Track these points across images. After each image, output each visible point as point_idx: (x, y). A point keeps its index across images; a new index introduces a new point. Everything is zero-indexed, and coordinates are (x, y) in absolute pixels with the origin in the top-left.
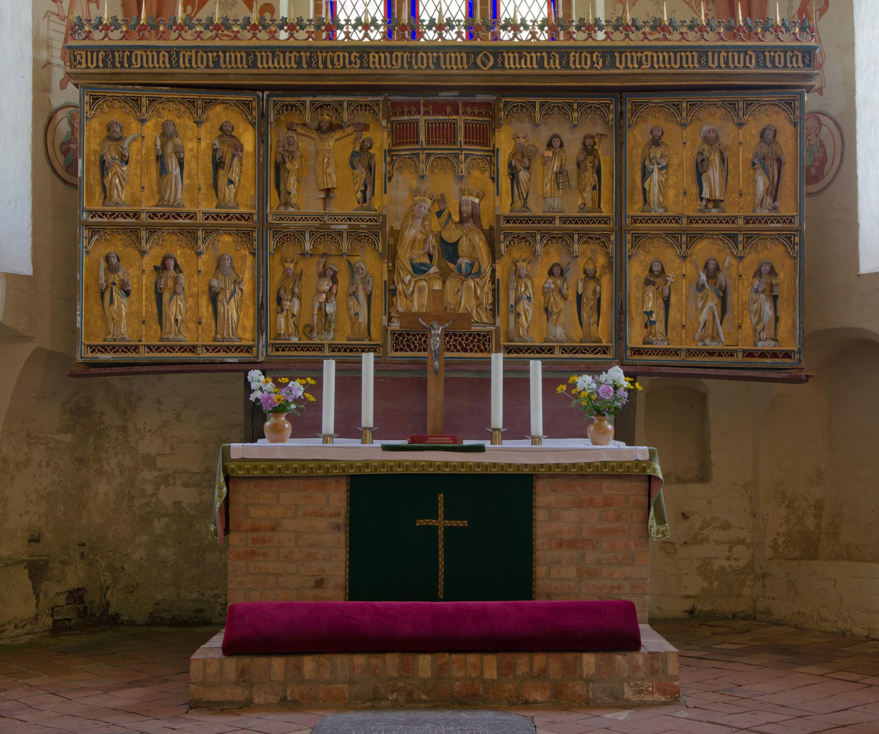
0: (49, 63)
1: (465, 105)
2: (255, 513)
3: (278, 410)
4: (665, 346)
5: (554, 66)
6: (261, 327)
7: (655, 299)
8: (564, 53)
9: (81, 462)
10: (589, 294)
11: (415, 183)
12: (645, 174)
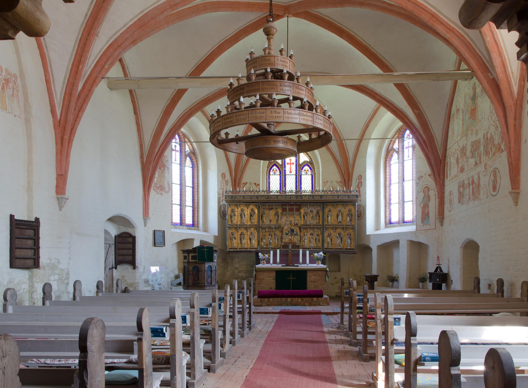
0: (220, 197)
1: (295, 205)
2: (260, 277)
3: (264, 260)
4: (331, 247)
5: (311, 198)
6: (259, 244)
7: (329, 239)
8: (313, 196)
9: (224, 269)
10: (318, 238)
11: (286, 218)
12: (328, 217)
